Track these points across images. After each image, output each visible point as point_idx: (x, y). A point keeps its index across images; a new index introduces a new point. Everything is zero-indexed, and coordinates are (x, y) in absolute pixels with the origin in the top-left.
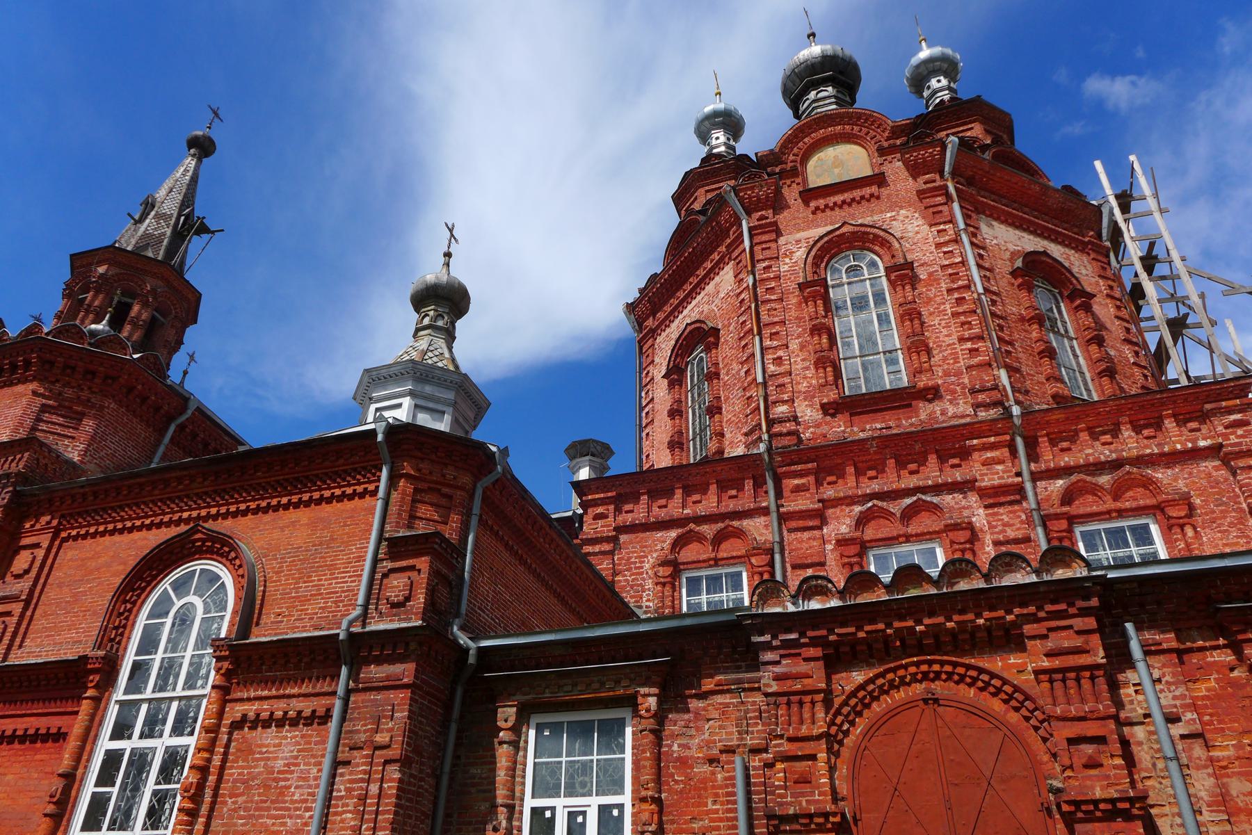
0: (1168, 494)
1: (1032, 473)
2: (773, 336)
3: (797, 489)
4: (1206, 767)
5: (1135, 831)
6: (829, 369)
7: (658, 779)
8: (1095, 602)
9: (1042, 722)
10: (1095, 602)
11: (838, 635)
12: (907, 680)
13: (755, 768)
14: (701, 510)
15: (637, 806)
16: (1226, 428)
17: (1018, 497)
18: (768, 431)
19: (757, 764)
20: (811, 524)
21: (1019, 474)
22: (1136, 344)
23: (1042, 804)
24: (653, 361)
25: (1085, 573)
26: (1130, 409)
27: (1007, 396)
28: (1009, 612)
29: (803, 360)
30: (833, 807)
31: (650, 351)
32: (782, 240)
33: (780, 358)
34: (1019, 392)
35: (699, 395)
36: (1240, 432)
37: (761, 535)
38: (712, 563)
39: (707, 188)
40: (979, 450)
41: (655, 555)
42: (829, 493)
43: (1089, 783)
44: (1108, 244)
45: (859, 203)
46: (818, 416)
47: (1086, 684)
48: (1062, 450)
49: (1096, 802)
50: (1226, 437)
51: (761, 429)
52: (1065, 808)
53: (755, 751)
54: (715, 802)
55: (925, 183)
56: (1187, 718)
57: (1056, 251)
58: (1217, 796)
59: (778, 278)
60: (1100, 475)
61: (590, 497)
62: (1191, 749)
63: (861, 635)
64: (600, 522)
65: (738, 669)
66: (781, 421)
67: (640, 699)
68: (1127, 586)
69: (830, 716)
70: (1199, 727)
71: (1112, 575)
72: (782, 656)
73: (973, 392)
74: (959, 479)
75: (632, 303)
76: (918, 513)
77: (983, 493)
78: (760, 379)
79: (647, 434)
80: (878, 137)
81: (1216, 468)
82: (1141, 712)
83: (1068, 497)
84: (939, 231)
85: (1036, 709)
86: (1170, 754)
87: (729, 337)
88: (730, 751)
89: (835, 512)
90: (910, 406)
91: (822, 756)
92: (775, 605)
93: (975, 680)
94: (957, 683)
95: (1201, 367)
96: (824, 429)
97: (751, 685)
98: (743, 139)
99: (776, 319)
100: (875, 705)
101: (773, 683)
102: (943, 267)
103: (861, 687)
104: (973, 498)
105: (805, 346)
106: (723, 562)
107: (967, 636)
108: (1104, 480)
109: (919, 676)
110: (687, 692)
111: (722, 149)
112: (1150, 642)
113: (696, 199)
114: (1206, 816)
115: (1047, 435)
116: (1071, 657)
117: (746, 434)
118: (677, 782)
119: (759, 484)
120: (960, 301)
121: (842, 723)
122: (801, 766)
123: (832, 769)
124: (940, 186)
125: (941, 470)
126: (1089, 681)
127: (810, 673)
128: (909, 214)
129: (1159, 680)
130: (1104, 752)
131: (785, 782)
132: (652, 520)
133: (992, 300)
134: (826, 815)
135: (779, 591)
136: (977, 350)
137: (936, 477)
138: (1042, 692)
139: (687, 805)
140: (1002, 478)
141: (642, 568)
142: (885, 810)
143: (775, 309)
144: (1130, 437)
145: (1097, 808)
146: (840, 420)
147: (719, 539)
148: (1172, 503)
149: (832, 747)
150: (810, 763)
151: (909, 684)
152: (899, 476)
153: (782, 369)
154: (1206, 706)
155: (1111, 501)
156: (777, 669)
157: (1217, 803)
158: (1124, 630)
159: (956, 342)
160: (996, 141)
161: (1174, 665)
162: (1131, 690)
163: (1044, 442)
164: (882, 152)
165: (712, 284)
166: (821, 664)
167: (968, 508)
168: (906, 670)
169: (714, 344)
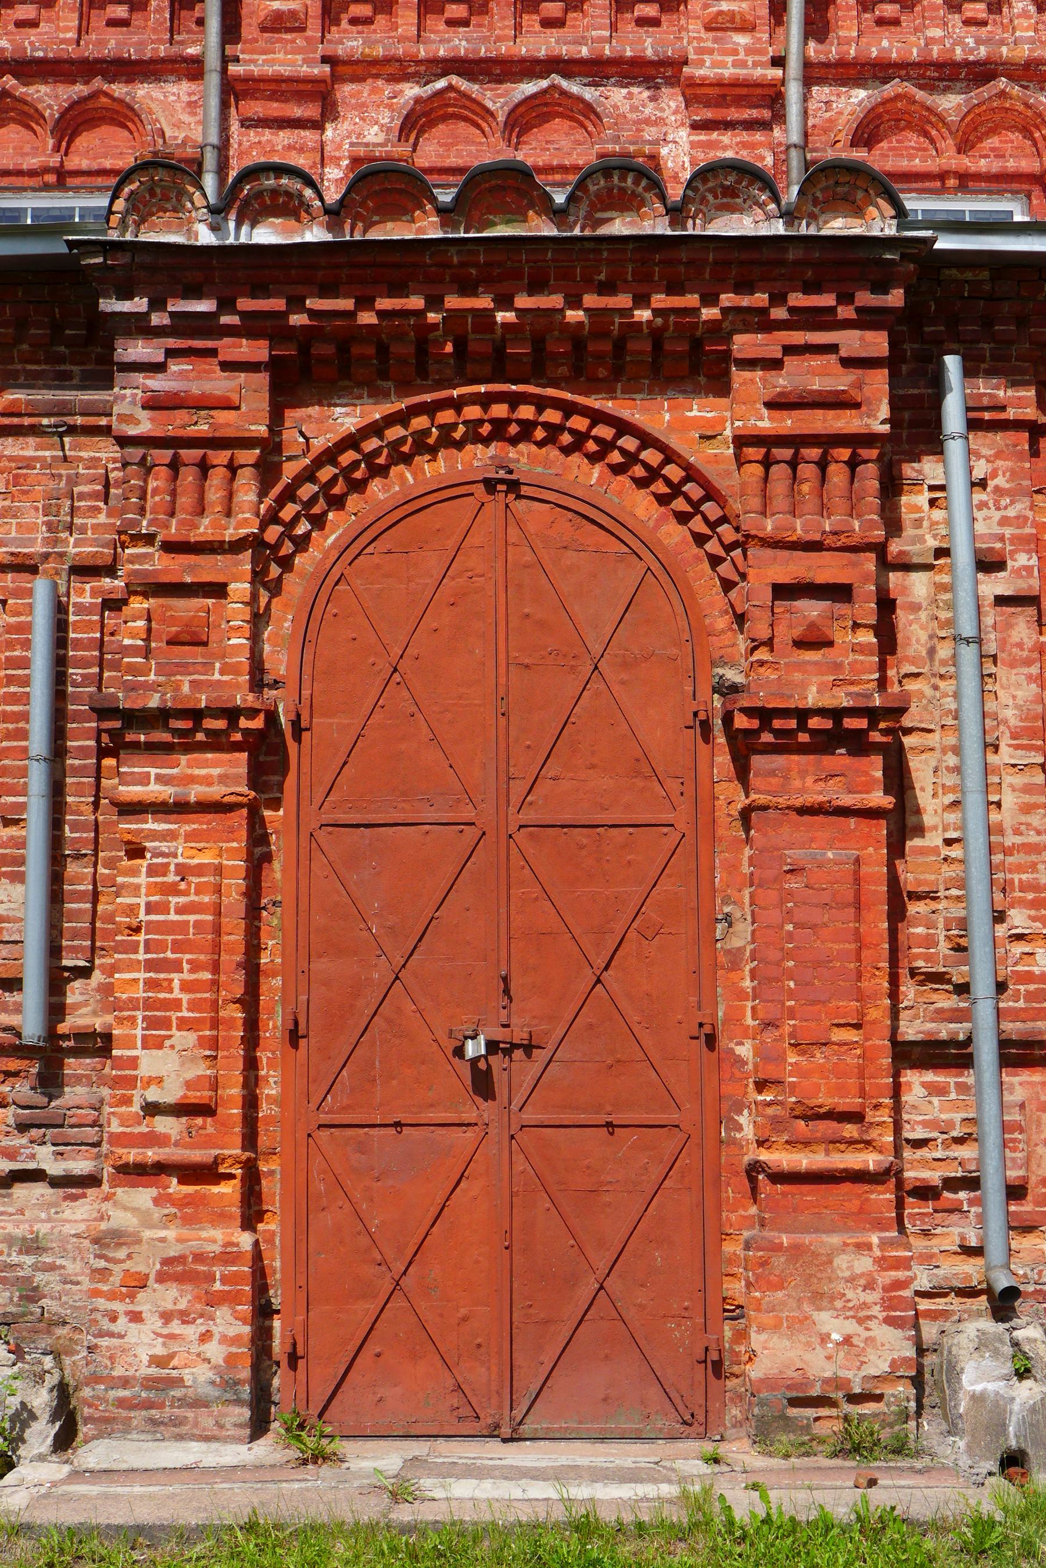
1: (807, 64)
4: (1028, 662)
5: (867, 774)
9: (729, 548)
10: (895, 298)
11: (313, 313)
12: (457, 435)
13: (81, 609)
17: (766, 114)
19: (87, 599)
20: (297, 111)
21: (779, 62)
23: (696, 714)
25: (890, 230)
28: (710, 299)
30: (251, 697)
37: (178, 125)
38: (51, 178)
43: (797, 676)
47: (837, 474)
48: (881, 22)
49: (803, 715)
52: (741, 722)
53: (84, 570)
56: (1017, 565)
60: (946, 90)
62: (1009, 626)
63: (367, 318)
65: (62, 380)
68: (969, 275)
69: (268, 501)
71: (945, 243)
72: (170, 353)
74: (649, 53)
76: (544, 118)
82: (932, 543)
85: (724, 520)
86: (968, 630)
89: (357, 95)
91: (240, 588)
92: (168, 228)
93: (606, 446)
94: (567, 451)
97: (91, 421)
101: (143, 415)
103: (351, 442)
104: (672, 101)
106: (77, 181)
107: (607, 346)
109: (486, 429)
112: (985, 401)
114: (1006, 755)
116: (819, 413)
123: (258, 619)
125: (613, 27)
126: (845, 469)
127: (235, 398)
129: (982, 484)
130: (842, 617)
131: (147, 640)
134: (232, 714)
135: (181, 193)
137: (601, 40)
138: (743, 485)
140: (743, 64)
142: (366, 709)
145: (802, 726)
149: (266, 571)
150: (210, 601)
151: (459, 445)
152: (518, 27)
155: (952, 151)
156: (157, 383)
157: (1032, 733)
158: (941, 368)
161: (1020, 456)
162: (922, 499)
166: (262, 379)
167: (659, 122)
168: (459, 412)
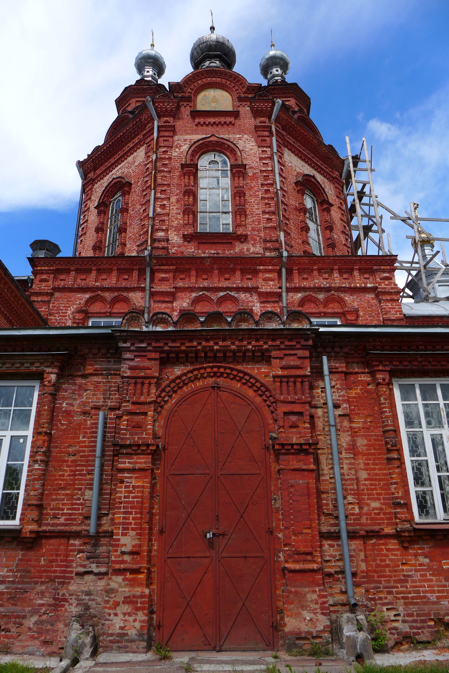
0: (349, 308)
1: (287, 288)
2: (162, 192)
3: (163, 279)
4: (348, 431)
6: (191, 216)
7: (52, 421)
8: (310, 342)
9: (272, 403)
10: (310, 342)
11: (170, 347)
12: (205, 376)
13: (111, 419)
14: (106, 284)
15: (35, 437)
16: (381, 279)
17: (278, 300)
18: (151, 245)
19: (112, 416)
20: (167, 300)
21: (280, 288)
22: (347, 235)
24: (90, 198)
25: (308, 327)
26: (340, 263)
27: (282, 246)
29: (177, 209)
30: (152, 441)
31: (89, 192)
32: (176, 138)
33: (164, 205)
34: (288, 245)
35: (115, 222)
36: (386, 283)
37: (139, 302)
38: (108, 314)
39: (137, 99)
40: (263, 272)
41: (75, 307)
42: (180, 284)
43: (291, 435)
44: (344, 181)
45: (222, 125)
46: (180, 241)
47: (298, 385)
48: (304, 279)
49: (292, 445)
50: (380, 284)
51: (147, 243)
52: (277, 447)
53: (112, 409)
54: (84, 437)
55: (260, 122)
57: (319, 178)
58: (351, 445)
59: (170, 159)
61: (39, 268)
63: (183, 348)
64: (44, 284)
66: (159, 240)
67: (45, 375)
68: (328, 337)
70: (348, 411)
72: (135, 356)
73: (265, 241)
74: (250, 286)
75: (82, 162)
77: (261, 294)
78: (151, 215)
79: (81, 241)
80: (239, 90)
81: (373, 299)
83: (302, 302)
84: (263, 151)
85: (271, 396)
87: (137, 189)
88: (97, 408)
90: (231, 243)
92: (136, 327)
93: (242, 378)
94: (232, 379)
95: (372, 251)
96: (183, 249)
98: (163, 76)
99: (165, 183)
100: (185, 388)
102: (261, 171)
103: (179, 377)
104: (255, 298)
105: (179, 201)
106: (114, 315)
107: (241, 354)
108: (321, 296)
110: (76, 373)
111: (150, 79)
112: (333, 367)
113: (129, 104)
114: (344, 455)
115: (298, 270)
116: (293, 370)
117: (138, 246)
118: (62, 424)
119: (142, 273)
120: (267, 191)
121: (165, 396)
122: (137, 418)
124: (268, 126)
125: (241, 280)
126: (300, 384)
127: (151, 367)
128: (249, 138)
132: (76, 286)
133: (283, 195)
134: (148, 445)
136: (271, 219)
137: (239, 283)
139: (67, 438)
140: (272, 288)
141: (66, 313)
143: (166, 177)
144: (337, 277)
146: (192, 245)
147: (115, 301)
148: (350, 312)
151: (205, 378)
152: (219, 280)
153: (164, 212)
154: (353, 402)
156: (132, 363)
157: (350, 449)
159: (261, 213)
160: (301, 110)
161: (343, 380)
162: (319, 391)
163: (296, 273)
164: (240, 99)
165: (132, 156)
166: (158, 362)
169: (127, 191)
